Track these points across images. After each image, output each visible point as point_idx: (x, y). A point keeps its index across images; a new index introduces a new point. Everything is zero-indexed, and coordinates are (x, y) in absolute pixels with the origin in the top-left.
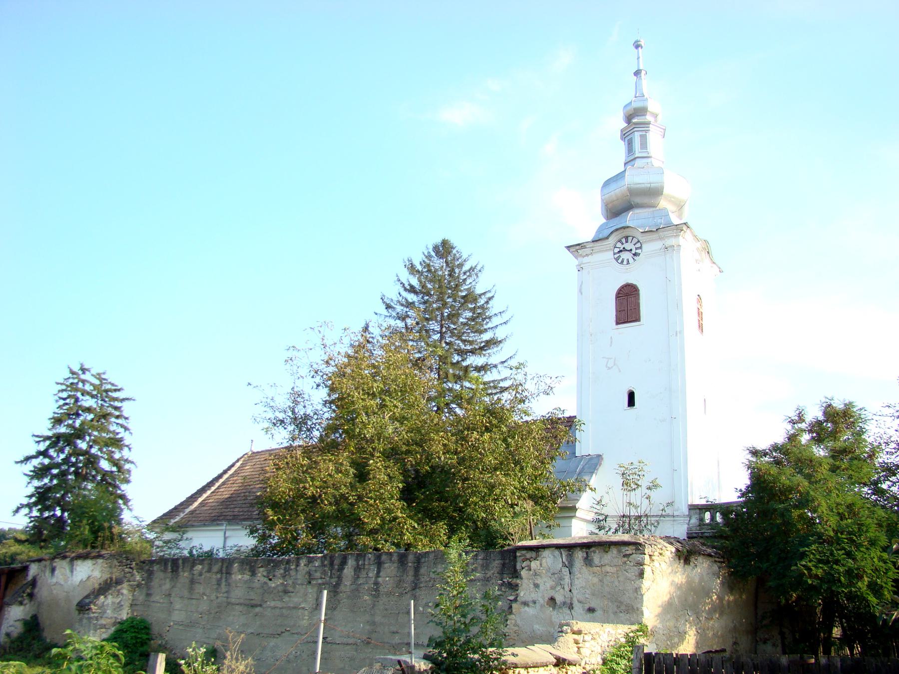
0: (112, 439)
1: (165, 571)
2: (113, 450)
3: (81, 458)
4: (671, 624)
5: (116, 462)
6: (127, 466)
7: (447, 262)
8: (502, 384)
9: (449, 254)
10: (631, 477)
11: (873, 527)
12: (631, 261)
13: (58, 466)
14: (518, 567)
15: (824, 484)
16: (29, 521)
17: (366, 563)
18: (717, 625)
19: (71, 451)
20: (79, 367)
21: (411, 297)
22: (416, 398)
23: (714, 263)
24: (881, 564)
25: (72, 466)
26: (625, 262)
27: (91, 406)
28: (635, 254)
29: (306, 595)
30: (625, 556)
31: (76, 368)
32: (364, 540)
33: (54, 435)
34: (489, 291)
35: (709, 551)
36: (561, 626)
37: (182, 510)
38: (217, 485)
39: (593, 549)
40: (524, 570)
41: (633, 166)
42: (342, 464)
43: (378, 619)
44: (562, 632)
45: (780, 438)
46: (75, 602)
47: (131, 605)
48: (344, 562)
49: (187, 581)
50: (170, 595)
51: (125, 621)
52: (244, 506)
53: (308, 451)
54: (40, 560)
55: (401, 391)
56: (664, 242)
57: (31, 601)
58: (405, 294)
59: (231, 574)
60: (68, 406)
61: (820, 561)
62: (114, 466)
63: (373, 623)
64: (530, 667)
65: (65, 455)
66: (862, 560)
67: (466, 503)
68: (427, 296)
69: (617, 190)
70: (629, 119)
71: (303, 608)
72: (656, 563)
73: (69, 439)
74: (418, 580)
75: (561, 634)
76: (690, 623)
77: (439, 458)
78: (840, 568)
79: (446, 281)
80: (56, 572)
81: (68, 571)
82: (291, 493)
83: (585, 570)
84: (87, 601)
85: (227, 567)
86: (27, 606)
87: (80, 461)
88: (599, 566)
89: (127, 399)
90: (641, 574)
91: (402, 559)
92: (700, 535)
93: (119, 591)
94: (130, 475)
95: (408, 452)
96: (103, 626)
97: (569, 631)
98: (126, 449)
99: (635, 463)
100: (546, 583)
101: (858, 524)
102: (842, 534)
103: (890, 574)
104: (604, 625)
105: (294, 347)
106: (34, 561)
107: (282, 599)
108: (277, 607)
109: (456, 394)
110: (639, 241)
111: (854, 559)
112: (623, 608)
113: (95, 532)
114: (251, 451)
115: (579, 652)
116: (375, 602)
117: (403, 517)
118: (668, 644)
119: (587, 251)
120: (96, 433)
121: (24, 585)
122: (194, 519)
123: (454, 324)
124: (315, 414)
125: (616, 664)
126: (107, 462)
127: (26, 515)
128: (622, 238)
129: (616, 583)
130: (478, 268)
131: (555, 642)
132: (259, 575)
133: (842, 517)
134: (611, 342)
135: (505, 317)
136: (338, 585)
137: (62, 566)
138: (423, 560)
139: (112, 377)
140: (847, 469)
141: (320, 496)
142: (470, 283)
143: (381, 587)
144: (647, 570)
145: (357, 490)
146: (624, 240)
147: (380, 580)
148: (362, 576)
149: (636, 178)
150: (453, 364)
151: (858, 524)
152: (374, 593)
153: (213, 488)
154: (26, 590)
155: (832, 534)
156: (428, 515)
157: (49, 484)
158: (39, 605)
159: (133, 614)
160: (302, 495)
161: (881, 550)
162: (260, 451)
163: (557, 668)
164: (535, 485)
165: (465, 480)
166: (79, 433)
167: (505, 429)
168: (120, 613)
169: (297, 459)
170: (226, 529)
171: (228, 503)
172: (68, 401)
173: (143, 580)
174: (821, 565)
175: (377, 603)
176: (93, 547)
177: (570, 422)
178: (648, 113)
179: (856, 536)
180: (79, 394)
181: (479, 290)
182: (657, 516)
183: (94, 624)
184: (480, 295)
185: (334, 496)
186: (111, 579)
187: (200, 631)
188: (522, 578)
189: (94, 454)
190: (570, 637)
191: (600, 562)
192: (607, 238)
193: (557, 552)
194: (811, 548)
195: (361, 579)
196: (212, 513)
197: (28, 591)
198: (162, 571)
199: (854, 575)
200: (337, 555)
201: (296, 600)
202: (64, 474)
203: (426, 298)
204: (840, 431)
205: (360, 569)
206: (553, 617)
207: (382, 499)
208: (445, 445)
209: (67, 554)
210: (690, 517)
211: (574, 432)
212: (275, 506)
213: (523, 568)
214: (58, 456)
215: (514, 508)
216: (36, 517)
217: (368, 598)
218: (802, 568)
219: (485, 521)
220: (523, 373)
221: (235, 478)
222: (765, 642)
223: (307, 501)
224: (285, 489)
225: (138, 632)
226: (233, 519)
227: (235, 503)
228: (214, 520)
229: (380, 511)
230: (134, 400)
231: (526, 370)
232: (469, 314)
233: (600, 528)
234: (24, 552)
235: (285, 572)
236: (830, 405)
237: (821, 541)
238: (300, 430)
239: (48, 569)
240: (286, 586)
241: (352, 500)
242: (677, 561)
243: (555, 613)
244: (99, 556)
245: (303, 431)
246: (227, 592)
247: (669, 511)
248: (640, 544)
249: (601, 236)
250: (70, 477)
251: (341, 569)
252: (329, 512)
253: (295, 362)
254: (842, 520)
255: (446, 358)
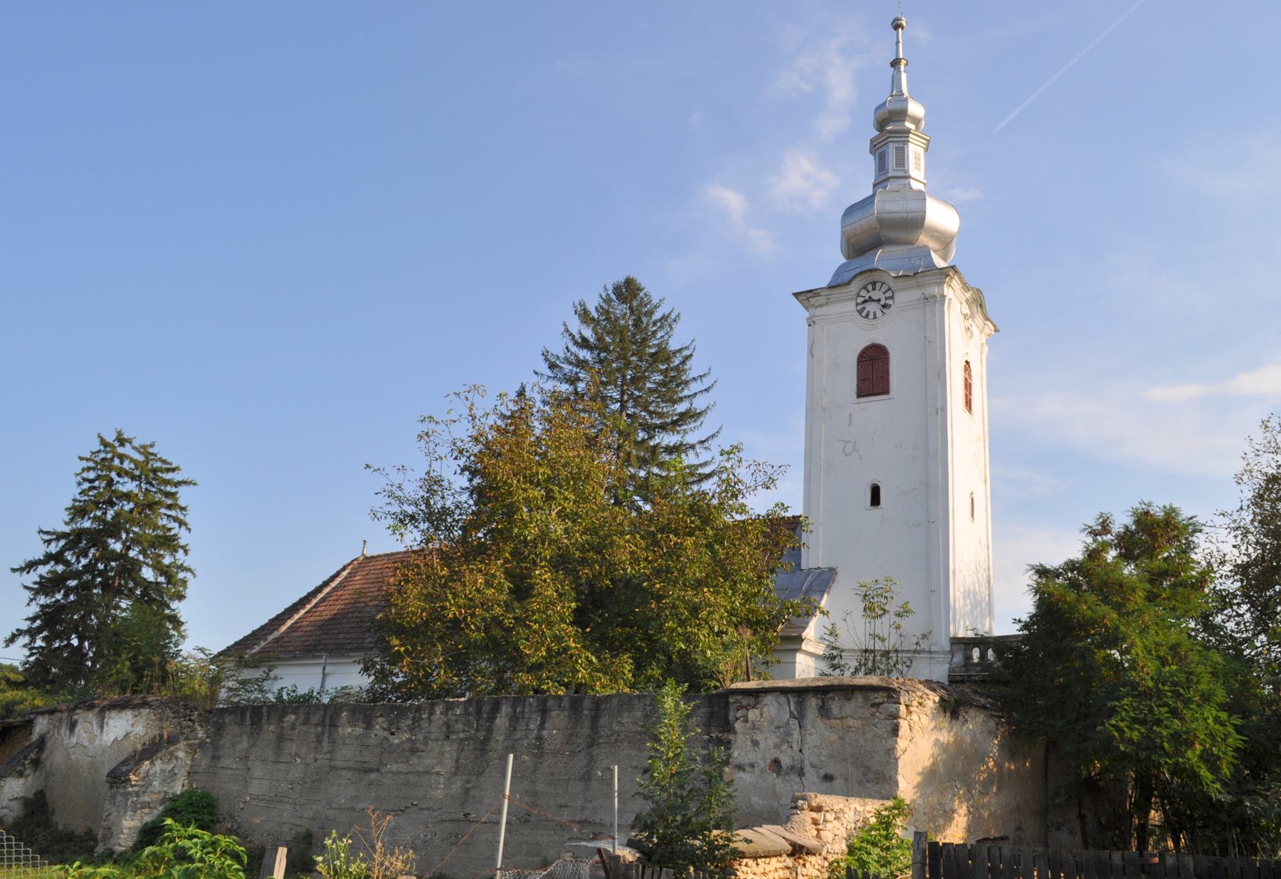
0: (161, 537)
1: (241, 723)
2: (162, 552)
3: (113, 564)
4: (934, 799)
5: (165, 569)
6: (181, 575)
7: (631, 308)
8: (701, 471)
9: (635, 297)
10: (876, 599)
11: (1206, 678)
12: (879, 314)
13: (77, 575)
14: (731, 718)
15: (1138, 616)
16: (28, 653)
17: (526, 710)
18: (993, 801)
19: (97, 554)
20: (114, 436)
21: (584, 354)
22: (593, 488)
23: (988, 319)
24: (1217, 727)
25: (99, 575)
26: (871, 316)
27: (131, 491)
28: (885, 306)
29: (443, 754)
30: (873, 705)
31: (110, 438)
32: (526, 678)
33: (73, 531)
34: (687, 348)
35: (983, 701)
36: (795, 799)
37: (264, 638)
38: (314, 601)
39: (830, 695)
40: (739, 721)
41: (885, 188)
42: (494, 576)
43: (540, 787)
44: (796, 808)
45: (1077, 554)
46: (106, 772)
47: (189, 772)
48: (495, 709)
49: (272, 737)
50: (247, 758)
51: (178, 796)
52: (351, 630)
53: (446, 558)
54: (51, 712)
55: (573, 478)
56: (923, 291)
57: (35, 771)
58: (574, 349)
59: (339, 727)
60: (96, 492)
61: (1135, 720)
62: (161, 575)
63: (534, 794)
64: (761, 857)
65: (88, 560)
66: (1192, 722)
67: (660, 629)
68: (605, 352)
69: (862, 221)
70: (881, 125)
71: (438, 773)
72: (915, 717)
73: (96, 538)
74: (596, 733)
75: (795, 811)
76: (959, 798)
77: (625, 570)
78: (1163, 731)
79: (629, 333)
80: (77, 729)
81: (95, 727)
82: (424, 614)
83: (819, 722)
84: (124, 769)
85: (331, 717)
86: (30, 778)
87: (112, 569)
88: (839, 719)
89: (185, 482)
90: (895, 731)
91: (575, 705)
92: (966, 678)
93: (171, 754)
94: (185, 588)
95: (583, 561)
96: (147, 805)
97: (806, 807)
98: (181, 551)
99: (880, 582)
100: (768, 740)
101: (1186, 673)
102: (1163, 684)
103: (1230, 740)
104: (850, 799)
105: (430, 417)
106: (42, 713)
107: (408, 761)
108: (401, 772)
109: (640, 482)
110: (890, 289)
111: (1182, 719)
112: (871, 776)
113: (138, 671)
114: (363, 554)
115: (818, 836)
116: (537, 763)
117: (576, 648)
118: (930, 827)
119: (822, 300)
120: (136, 529)
121: (26, 748)
122: (280, 649)
123: (639, 390)
124: (457, 507)
125: (866, 853)
126: (151, 569)
127: (25, 646)
128: (860, 291)
129: (862, 742)
130: (673, 316)
131: (786, 822)
132: (377, 727)
133: (1163, 661)
134: (851, 421)
135: (706, 383)
136: (487, 739)
137: (86, 721)
138: (603, 706)
139: (163, 451)
140: (1169, 599)
141: (466, 618)
142: (662, 337)
143: (546, 744)
144: (904, 724)
145: (515, 611)
146: (870, 287)
147: (545, 733)
148: (520, 728)
149: (887, 205)
150: (637, 443)
151: (1186, 673)
152: (536, 751)
153: (308, 607)
154: (29, 755)
155: (1151, 684)
156: (602, 643)
157: (62, 601)
158: (49, 775)
159: (191, 786)
160: (441, 618)
161: (1217, 708)
162: (375, 555)
163: (792, 859)
164: (747, 607)
165: (659, 598)
166: (113, 529)
167: (711, 533)
168: (172, 784)
169: (433, 569)
170: (325, 663)
171: (330, 627)
172: (96, 484)
173: (207, 738)
174: (1136, 726)
175: (539, 765)
176: (134, 692)
177: (794, 524)
178: (907, 118)
179: (1182, 688)
180: (113, 475)
181: (673, 345)
182: (908, 651)
183: (132, 802)
184: (675, 353)
185: (484, 619)
186: (161, 736)
187: (289, 807)
188: (735, 733)
189: (133, 558)
190: (808, 816)
191: (841, 713)
192: (848, 283)
193: (783, 699)
194: (1123, 702)
195: (518, 732)
196: (306, 641)
197: (33, 756)
198: (236, 723)
199: (1182, 741)
200: (486, 699)
201: (428, 761)
202: (86, 587)
203: (603, 355)
204: (1160, 547)
205: (518, 718)
206: (777, 786)
207: (550, 624)
208: (632, 553)
209: (96, 702)
210: (952, 653)
211: (800, 536)
212: (400, 631)
213: (737, 719)
214: (79, 562)
215: (722, 638)
216: (41, 647)
217: (527, 758)
218: (1112, 728)
219: (683, 654)
220: (737, 459)
221: (340, 593)
222: (1058, 828)
223: (445, 625)
224: (417, 608)
225: (196, 812)
226: (337, 649)
227: (339, 626)
228: (309, 651)
229: (546, 639)
230: (195, 484)
231: (741, 455)
232: (658, 377)
233: (834, 667)
234: (26, 700)
235: (413, 724)
236: (1147, 513)
237: (1137, 693)
238: (437, 529)
239: (64, 723)
240: (414, 742)
241: (508, 624)
242: (942, 714)
243: (780, 780)
244: (145, 704)
245: (440, 530)
246: (330, 752)
247: (924, 645)
248: (894, 690)
249: (839, 281)
250: (95, 591)
251: (492, 717)
252: (476, 641)
253: (432, 438)
254: (1163, 666)
255: (628, 434)
